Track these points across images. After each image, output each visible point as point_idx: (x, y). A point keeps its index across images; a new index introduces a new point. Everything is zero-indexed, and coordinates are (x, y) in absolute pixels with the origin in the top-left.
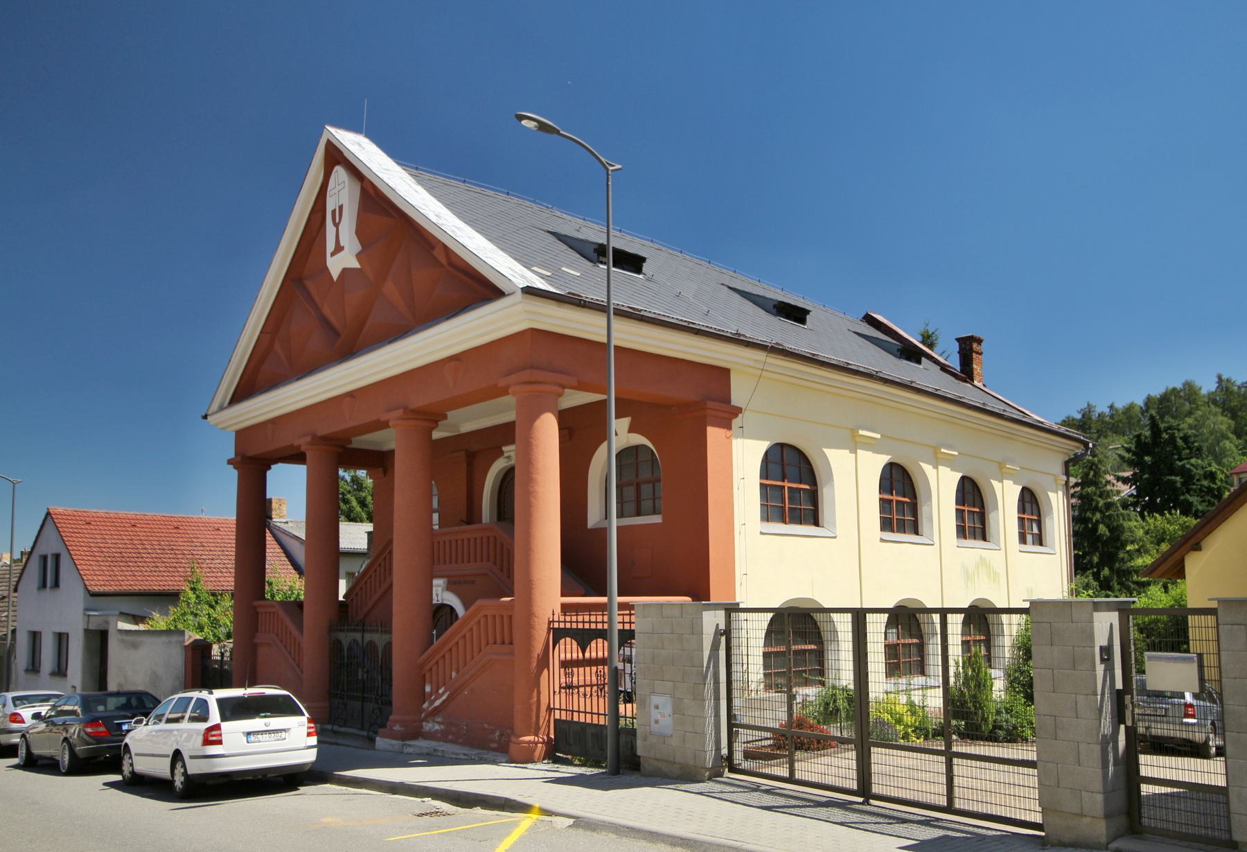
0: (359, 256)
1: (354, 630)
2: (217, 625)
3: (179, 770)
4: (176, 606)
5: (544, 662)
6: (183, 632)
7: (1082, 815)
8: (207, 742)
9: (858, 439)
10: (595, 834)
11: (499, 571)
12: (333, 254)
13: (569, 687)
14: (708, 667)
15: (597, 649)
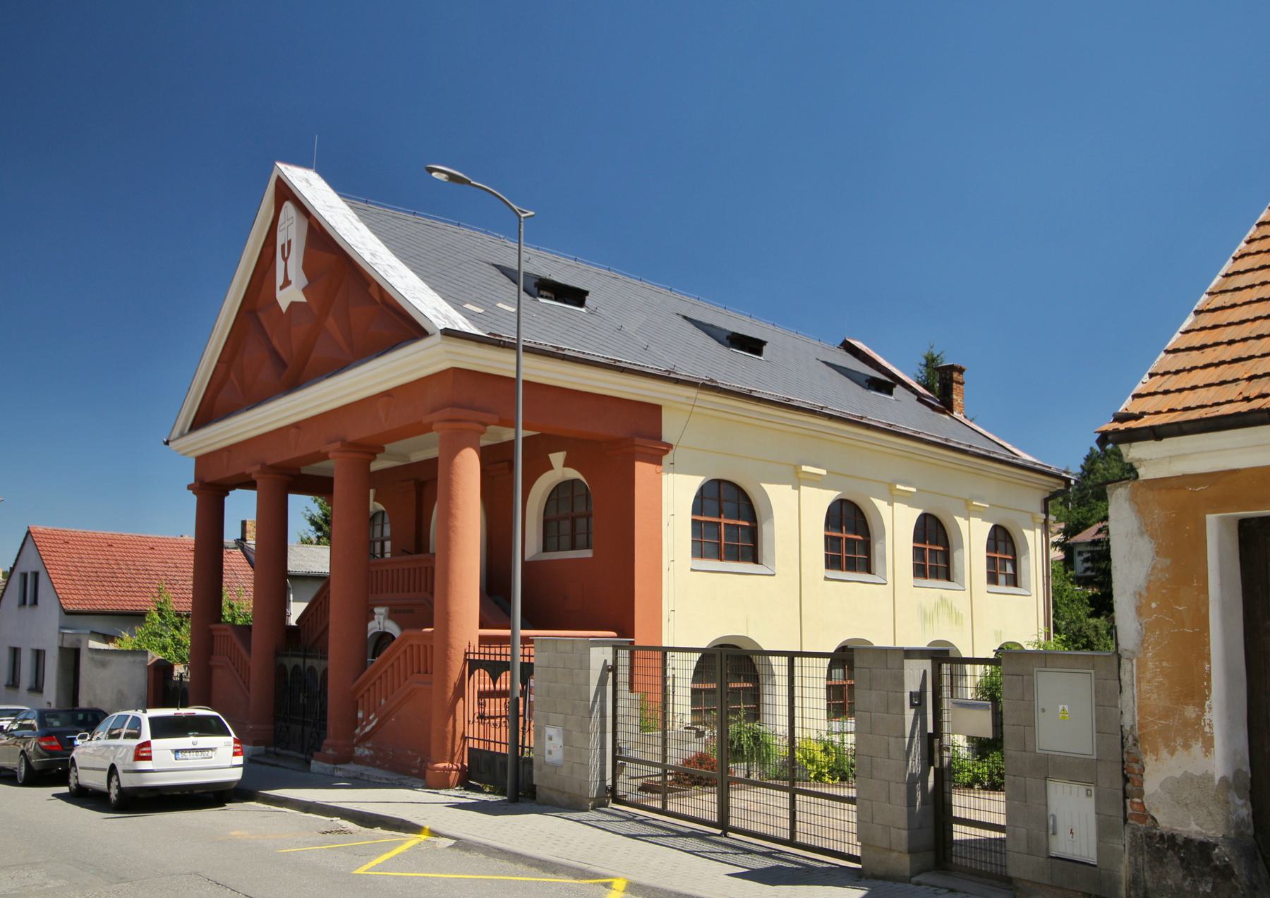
0: (305, 291)
1: (297, 656)
2: (174, 647)
3: (114, 783)
4: (141, 625)
5: (460, 691)
6: (146, 653)
7: (891, 850)
8: (138, 758)
9: (801, 476)
10: (467, 854)
11: (422, 601)
12: (282, 288)
13: (482, 717)
14: (595, 701)
15: (504, 683)
